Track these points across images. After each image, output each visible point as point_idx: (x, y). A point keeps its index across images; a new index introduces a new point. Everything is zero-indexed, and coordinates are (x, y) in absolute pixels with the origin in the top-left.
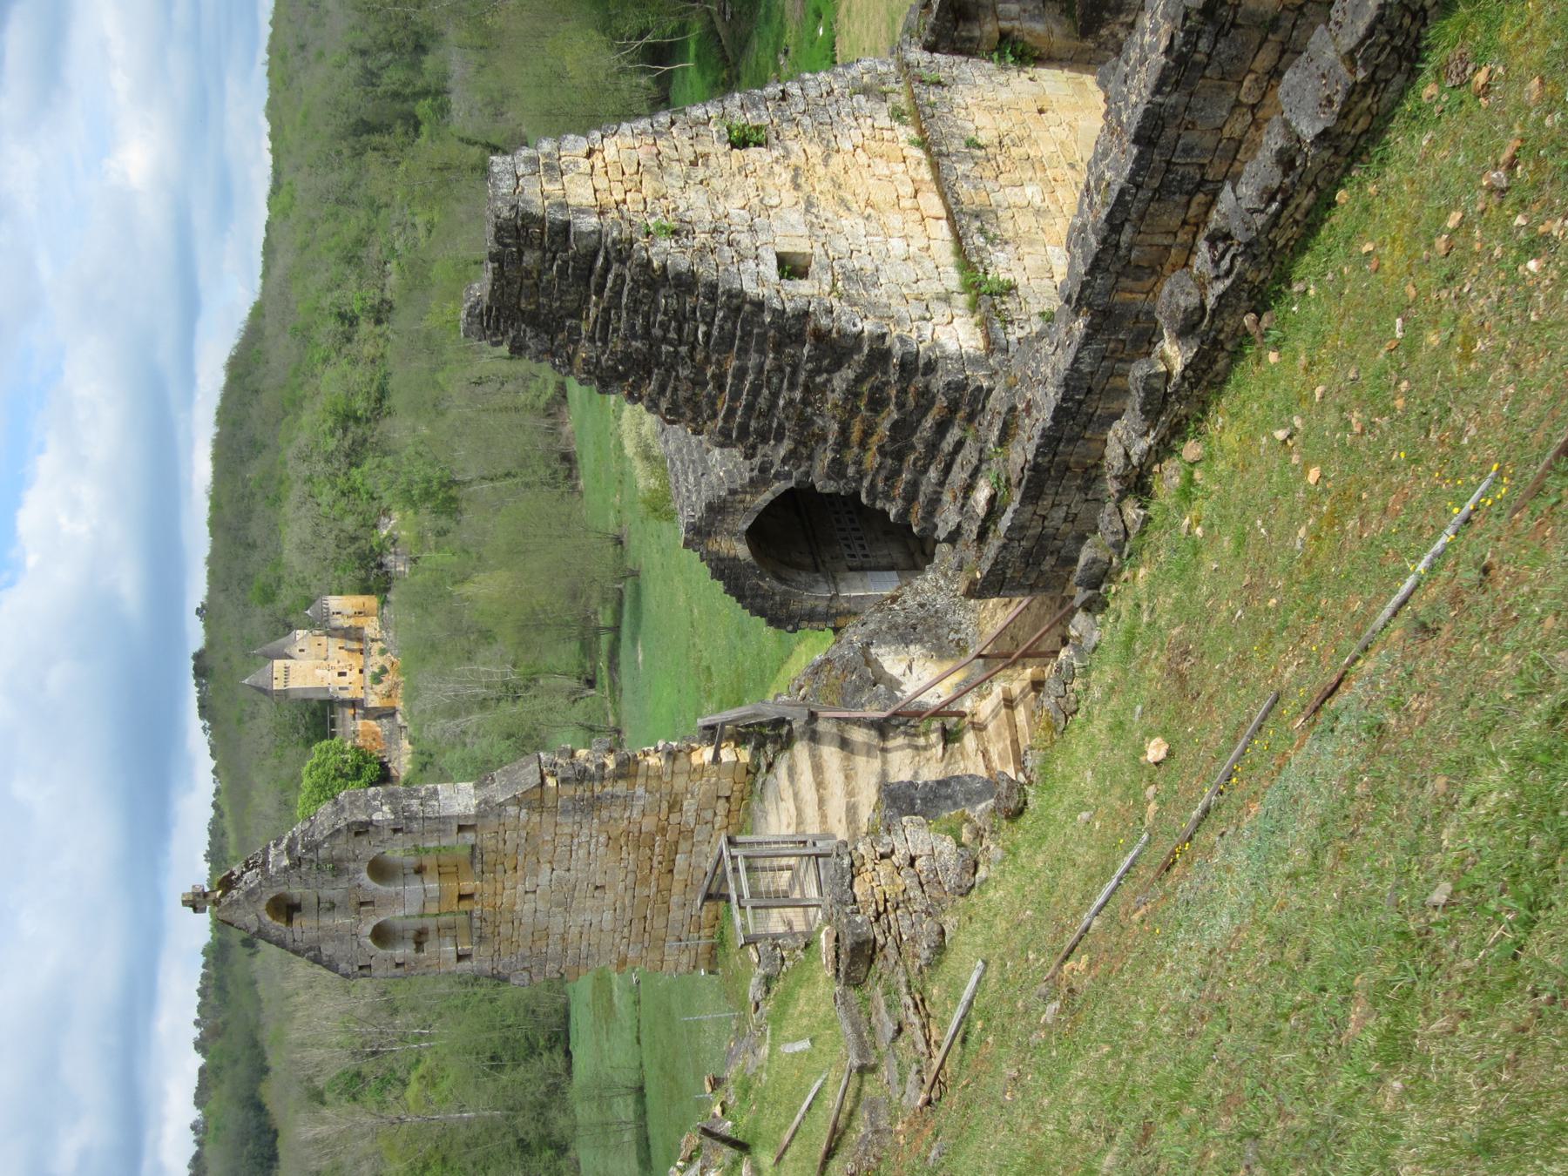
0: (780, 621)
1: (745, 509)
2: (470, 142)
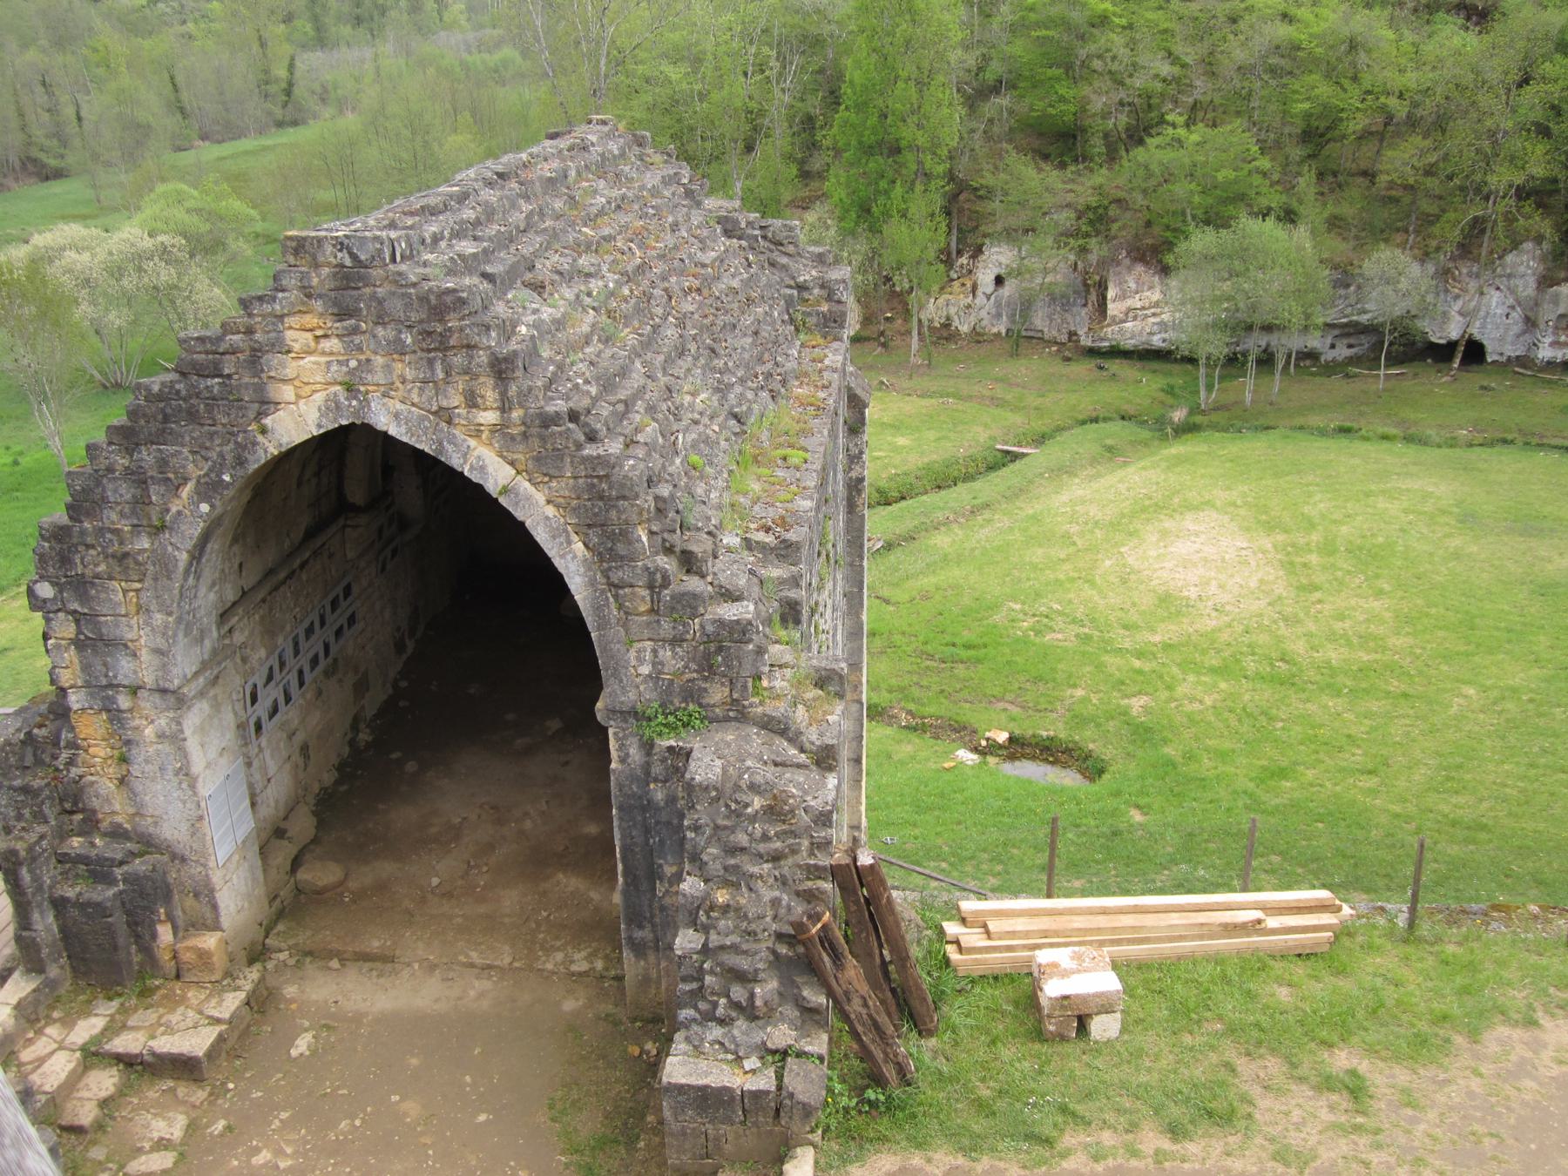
0: (65, 560)
1: (445, 415)
2: (291, 67)
